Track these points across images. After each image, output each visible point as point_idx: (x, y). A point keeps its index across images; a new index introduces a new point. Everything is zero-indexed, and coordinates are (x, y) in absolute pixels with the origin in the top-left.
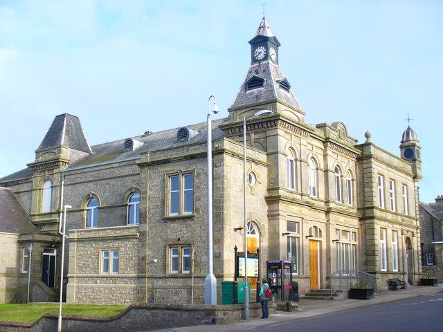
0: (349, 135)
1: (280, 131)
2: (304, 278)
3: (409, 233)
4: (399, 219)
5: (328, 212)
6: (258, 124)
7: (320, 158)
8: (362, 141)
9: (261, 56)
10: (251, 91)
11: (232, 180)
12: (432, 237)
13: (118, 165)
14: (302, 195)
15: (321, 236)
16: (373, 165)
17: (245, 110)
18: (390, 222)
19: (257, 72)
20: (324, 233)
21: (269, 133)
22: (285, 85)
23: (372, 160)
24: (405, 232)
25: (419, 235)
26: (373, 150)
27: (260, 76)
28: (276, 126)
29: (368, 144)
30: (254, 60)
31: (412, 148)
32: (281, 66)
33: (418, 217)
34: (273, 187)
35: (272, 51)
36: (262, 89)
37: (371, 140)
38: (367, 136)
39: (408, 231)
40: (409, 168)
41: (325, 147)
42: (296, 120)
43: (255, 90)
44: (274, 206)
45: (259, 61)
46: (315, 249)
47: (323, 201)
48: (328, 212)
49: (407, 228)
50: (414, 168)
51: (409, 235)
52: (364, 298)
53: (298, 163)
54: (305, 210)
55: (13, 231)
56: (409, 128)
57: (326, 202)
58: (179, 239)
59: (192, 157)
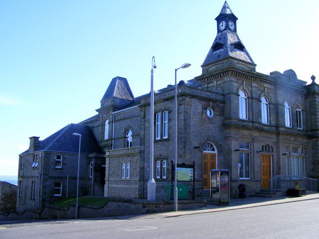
5: (278, 134)
8: (309, 82)
9: (222, 28)
10: (215, 52)
11: (192, 113)
14: (253, 122)
15: (272, 151)
19: (220, 39)
27: (221, 42)
29: (314, 84)
30: (219, 31)
32: (244, 32)
35: (230, 23)
36: (222, 50)
38: (313, 78)
43: (218, 52)
44: (228, 131)
45: (222, 31)
46: (139, 108)
48: (278, 134)
55: (20, 176)
57: (276, 127)
58: (161, 155)
59: (167, 99)
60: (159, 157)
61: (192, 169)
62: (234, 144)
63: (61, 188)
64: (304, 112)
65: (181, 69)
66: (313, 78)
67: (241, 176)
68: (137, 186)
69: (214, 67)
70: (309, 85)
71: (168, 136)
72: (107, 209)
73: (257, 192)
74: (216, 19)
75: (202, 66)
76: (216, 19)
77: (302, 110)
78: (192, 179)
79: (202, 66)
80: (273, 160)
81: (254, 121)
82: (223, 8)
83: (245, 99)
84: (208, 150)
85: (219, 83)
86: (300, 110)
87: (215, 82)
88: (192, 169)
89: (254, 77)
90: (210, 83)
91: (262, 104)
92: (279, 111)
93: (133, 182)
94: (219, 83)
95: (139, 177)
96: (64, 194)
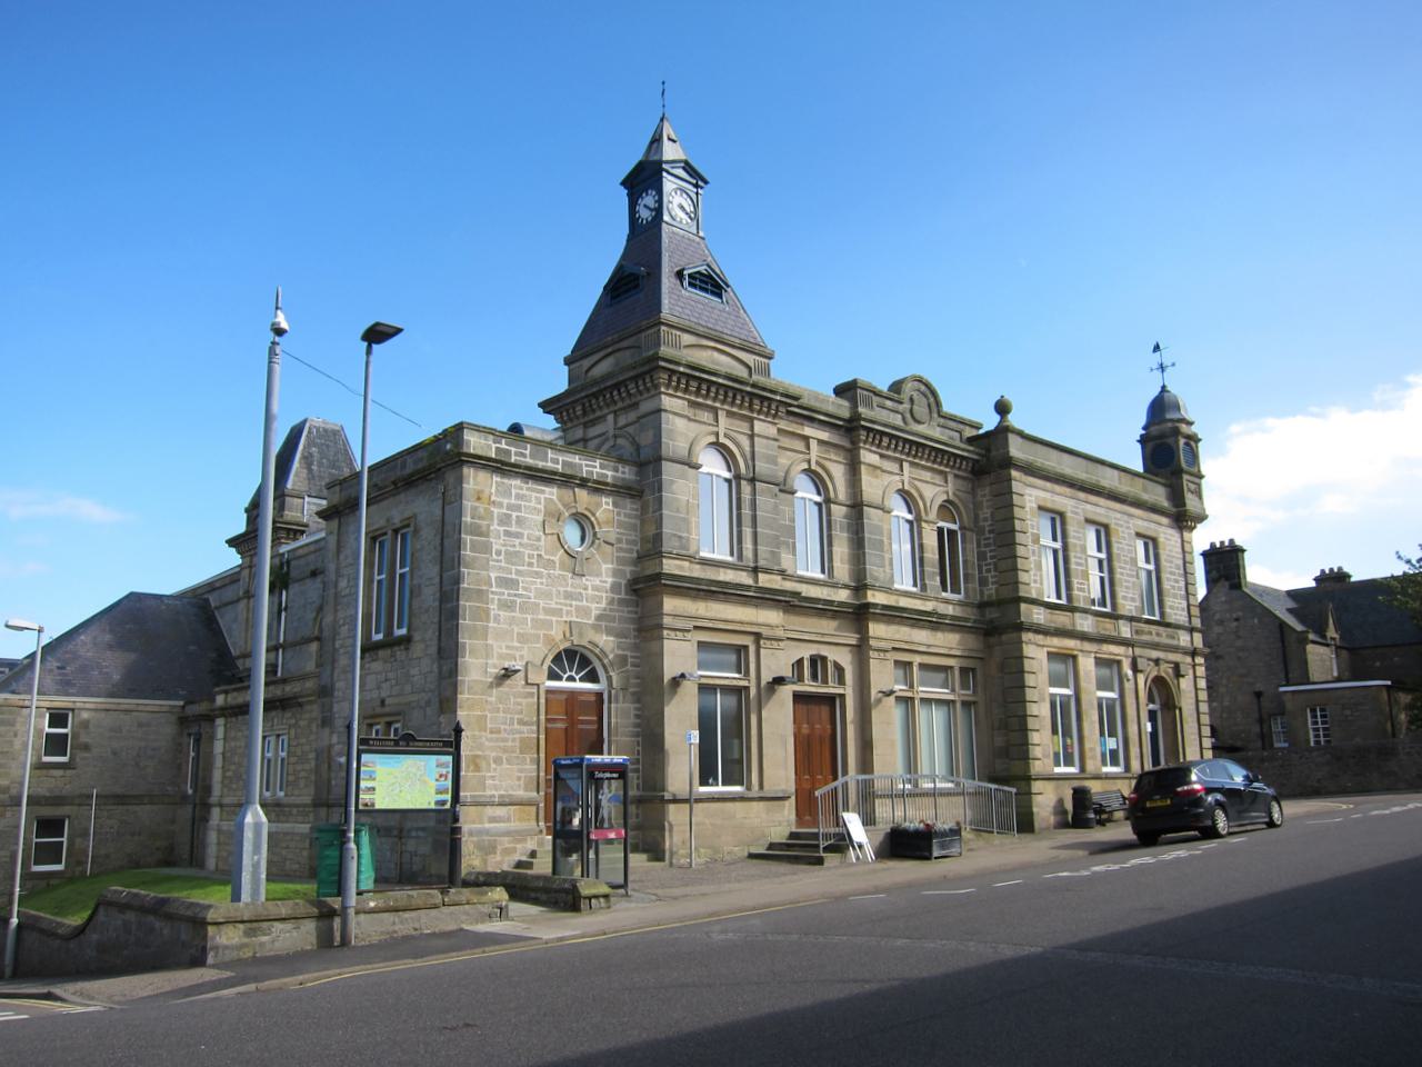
0: (947, 408)
1: (671, 402)
2: (762, 799)
3: (1164, 666)
4: (1125, 631)
6: (617, 386)
7: (838, 472)
8: (990, 422)
12: (1282, 676)
13: (747, 531)
14: (755, 570)
15: (841, 681)
16: (1016, 486)
17: (602, 354)
18: (1084, 637)
20: (849, 676)
21: (646, 407)
22: (710, 283)
23: (1014, 473)
24: (1141, 664)
25: (1201, 671)
26: (1016, 449)
28: (657, 387)
29: (1002, 431)
31: (1170, 441)
33: (1197, 622)
34: (649, 547)
37: (1014, 420)
38: (1002, 408)
39: (1157, 662)
40: (1157, 494)
41: (855, 443)
42: (742, 372)
47: (846, 587)
49: (1155, 654)
50: (1177, 496)
51: (1166, 671)
52: (924, 855)
53: (746, 488)
54: (771, 617)
56: (1164, 387)
60: (379, 710)
61: (449, 759)
62: (678, 656)
63: (65, 839)
64: (968, 534)
65: (372, 358)
66: (1002, 408)
67: (1057, 764)
68: (305, 828)
69: (610, 360)
70: (988, 434)
71: (409, 630)
72: (95, 937)
73: (777, 840)
74: (624, 183)
75: (568, 361)
76: (624, 183)
77: (960, 528)
78: (443, 803)
79: (568, 361)
80: (609, 717)
81: (761, 563)
82: (652, 143)
83: (728, 481)
84: (571, 679)
85: (622, 421)
86: (954, 527)
87: (610, 418)
88: (449, 759)
89: (763, 399)
90: (593, 423)
91: (798, 505)
92: (666, 530)
93: (295, 811)
94: (622, 421)
95: (312, 790)
96: (76, 859)
